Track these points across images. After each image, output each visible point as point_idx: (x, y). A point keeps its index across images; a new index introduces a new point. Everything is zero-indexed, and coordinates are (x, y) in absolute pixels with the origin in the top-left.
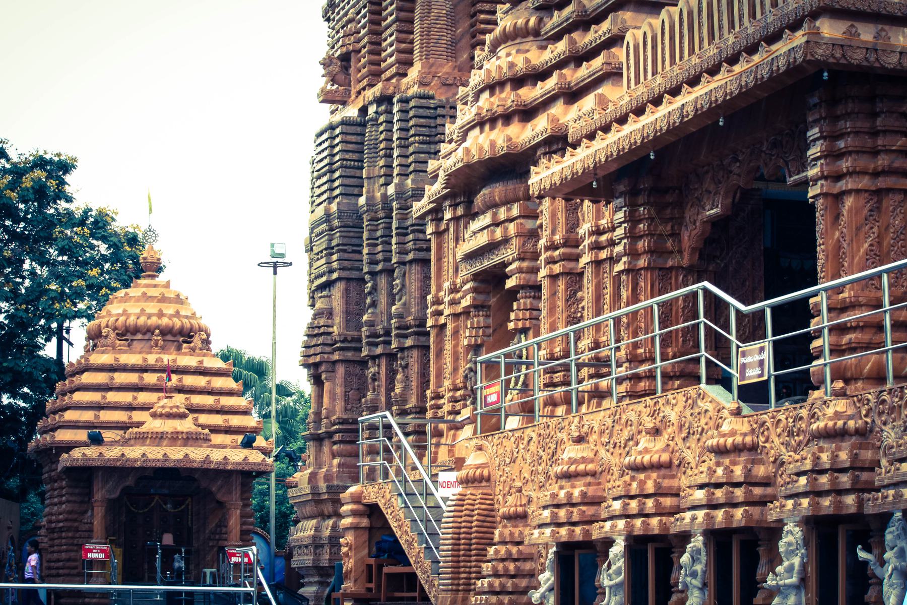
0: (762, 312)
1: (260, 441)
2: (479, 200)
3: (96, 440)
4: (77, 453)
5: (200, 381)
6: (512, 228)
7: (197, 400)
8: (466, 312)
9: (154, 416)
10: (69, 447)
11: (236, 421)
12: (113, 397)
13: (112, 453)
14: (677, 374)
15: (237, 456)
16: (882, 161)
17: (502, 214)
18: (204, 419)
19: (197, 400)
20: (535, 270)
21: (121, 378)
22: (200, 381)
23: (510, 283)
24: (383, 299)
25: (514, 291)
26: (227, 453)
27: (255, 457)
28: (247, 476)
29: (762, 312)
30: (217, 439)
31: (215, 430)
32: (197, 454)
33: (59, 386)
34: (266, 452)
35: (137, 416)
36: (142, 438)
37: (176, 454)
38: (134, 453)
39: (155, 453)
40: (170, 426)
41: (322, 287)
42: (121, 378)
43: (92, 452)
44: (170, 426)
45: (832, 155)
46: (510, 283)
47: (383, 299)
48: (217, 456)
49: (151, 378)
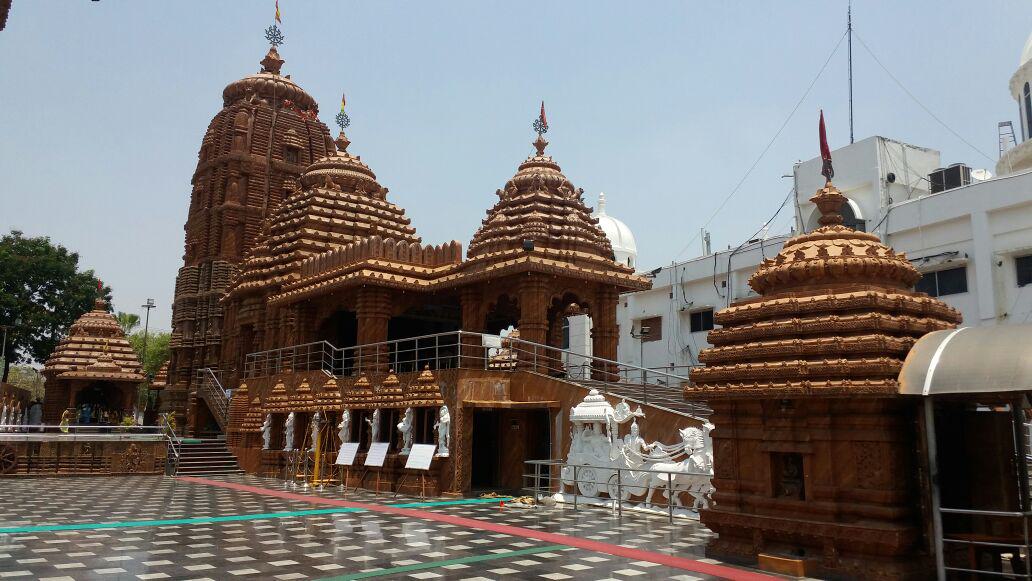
0: (944, 515)
1: (142, 371)
2: (245, 302)
3: (75, 369)
4: (65, 374)
5: (118, 349)
6: (257, 312)
7: (116, 355)
8: (237, 336)
9: (99, 361)
10: (62, 371)
11: (131, 363)
12: (81, 353)
13: (81, 374)
14: (889, 501)
15: (132, 376)
16: (378, 309)
17: (253, 307)
18: (118, 362)
19: (116, 355)
20: (263, 326)
21: (85, 346)
22: (118, 349)
23: (254, 329)
24: (203, 328)
25: (256, 332)
26: (127, 374)
27: (140, 377)
28: (135, 383)
29: (944, 515)
30: (123, 370)
31: (124, 366)
32: (117, 375)
33: (56, 347)
34: (143, 375)
35: (91, 361)
36: (90, 370)
37: (108, 375)
38: (91, 374)
39: (99, 375)
40: (104, 365)
41: (179, 322)
42: (85, 346)
43: (73, 374)
44: (104, 365)
45: (364, 307)
46: (254, 329)
47: (203, 328)
48: (124, 376)
49: (97, 347)
